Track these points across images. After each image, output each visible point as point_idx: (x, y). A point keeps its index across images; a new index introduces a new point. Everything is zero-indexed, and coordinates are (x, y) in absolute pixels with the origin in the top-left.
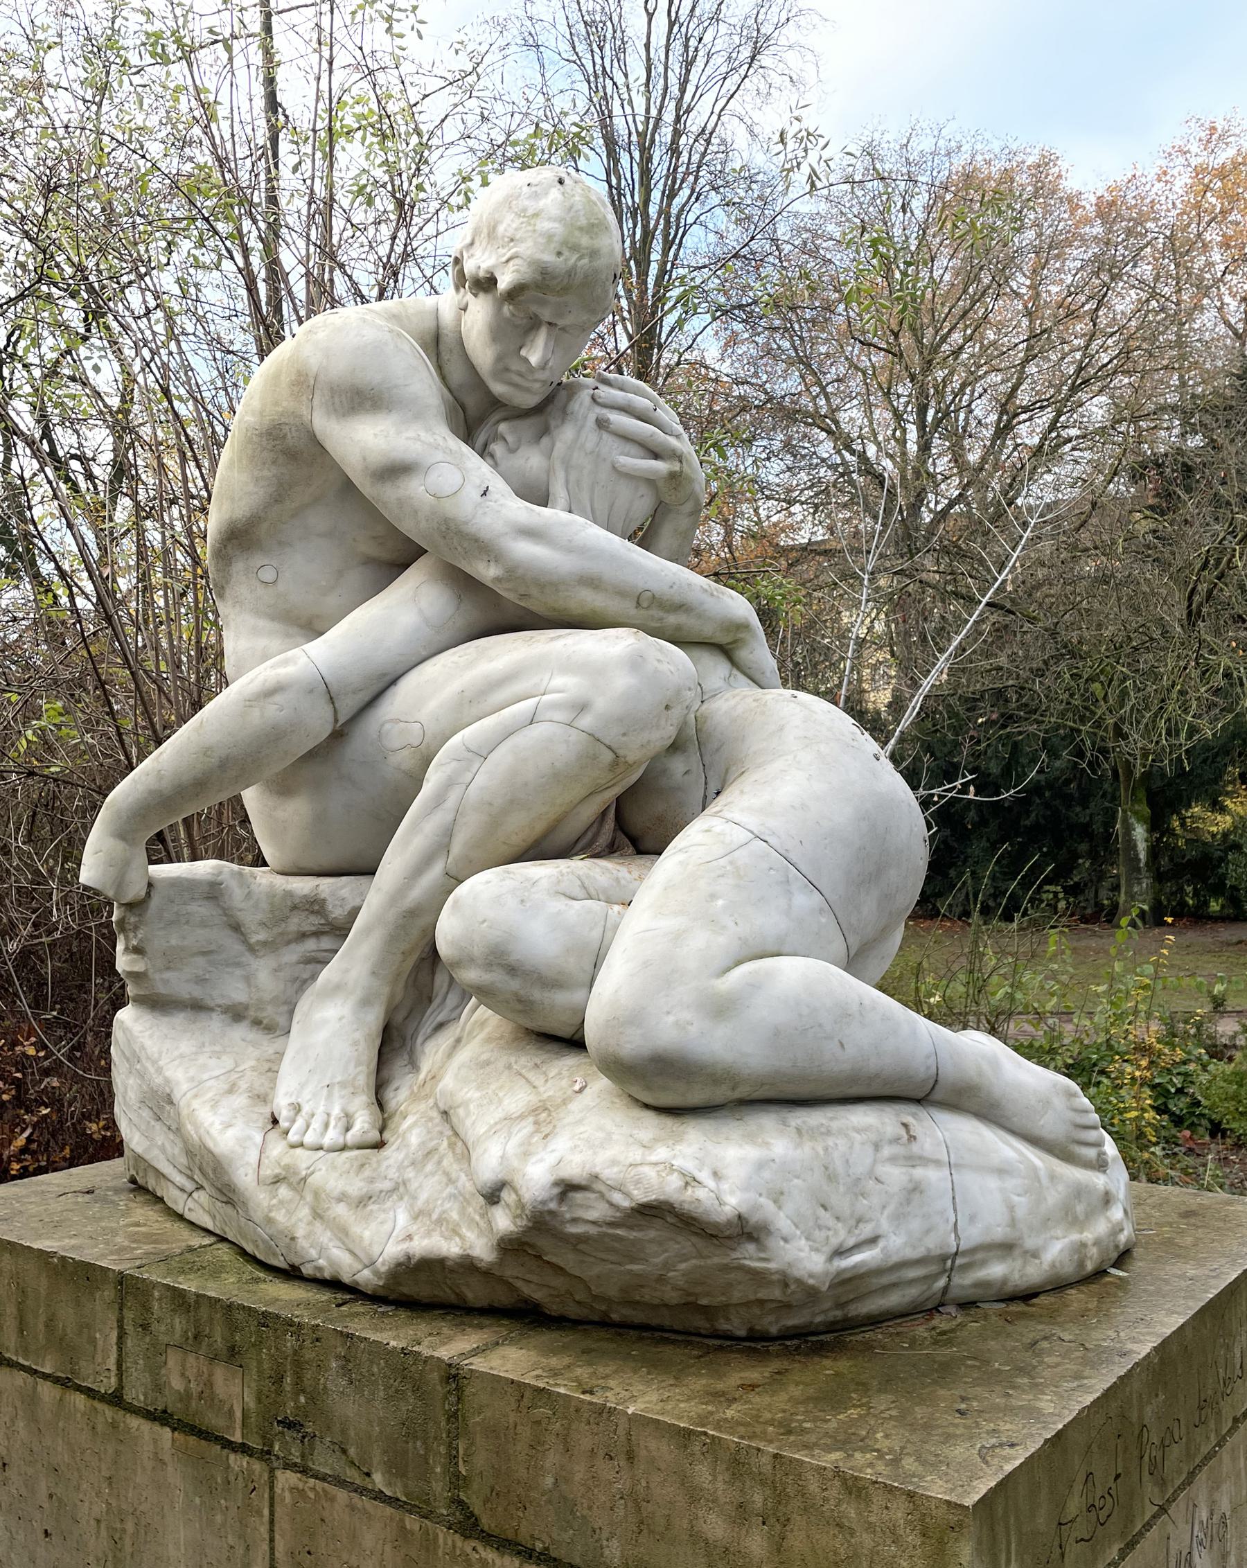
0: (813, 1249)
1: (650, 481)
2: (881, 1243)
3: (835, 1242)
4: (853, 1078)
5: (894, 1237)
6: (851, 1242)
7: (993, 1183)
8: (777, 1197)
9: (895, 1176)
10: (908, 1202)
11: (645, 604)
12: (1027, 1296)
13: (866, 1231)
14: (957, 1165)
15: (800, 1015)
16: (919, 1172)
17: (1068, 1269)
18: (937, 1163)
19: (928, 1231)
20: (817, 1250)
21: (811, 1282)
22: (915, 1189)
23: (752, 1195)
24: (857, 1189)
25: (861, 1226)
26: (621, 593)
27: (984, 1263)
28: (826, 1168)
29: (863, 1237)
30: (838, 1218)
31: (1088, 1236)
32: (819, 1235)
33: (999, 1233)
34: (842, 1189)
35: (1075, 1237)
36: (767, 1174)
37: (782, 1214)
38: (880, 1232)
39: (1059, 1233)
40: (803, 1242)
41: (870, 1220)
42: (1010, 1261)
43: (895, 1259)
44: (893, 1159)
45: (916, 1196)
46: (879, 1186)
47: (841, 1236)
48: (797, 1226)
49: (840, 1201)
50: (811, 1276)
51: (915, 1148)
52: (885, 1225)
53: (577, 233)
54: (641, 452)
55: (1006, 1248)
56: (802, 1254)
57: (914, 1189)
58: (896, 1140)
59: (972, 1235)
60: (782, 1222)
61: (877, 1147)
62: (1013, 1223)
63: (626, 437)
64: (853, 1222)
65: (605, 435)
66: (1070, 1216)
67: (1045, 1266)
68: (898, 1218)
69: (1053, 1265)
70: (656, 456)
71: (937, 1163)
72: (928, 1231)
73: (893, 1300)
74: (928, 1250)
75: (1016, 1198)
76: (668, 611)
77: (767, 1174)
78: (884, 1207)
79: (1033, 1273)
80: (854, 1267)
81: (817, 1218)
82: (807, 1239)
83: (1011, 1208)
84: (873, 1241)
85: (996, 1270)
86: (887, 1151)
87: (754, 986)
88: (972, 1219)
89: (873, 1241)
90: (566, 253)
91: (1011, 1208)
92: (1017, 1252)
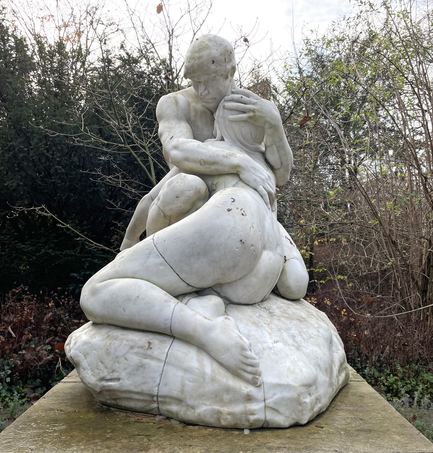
0: (93, 375)
1: (245, 121)
2: (121, 381)
3: (102, 375)
4: (140, 323)
5: (127, 381)
6: (109, 377)
7: (180, 373)
8: (86, 355)
9: (135, 359)
10: (137, 370)
11: (203, 164)
12: (187, 423)
13: (115, 375)
14: (168, 363)
15: (112, 298)
16: (147, 361)
17: (211, 420)
18: (159, 360)
19: (144, 383)
20: (94, 376)
21: (90, 385)
22: (142, 366)
23: (77, 352)
24: (116, 359)
25: (114, 373)
26: (195, 161)
27: (170, 404)
28: (107, 350)
29: (113, 377)
30: (106, 368)
31: (225, 409)
32: (96, 371)
33: (175, 393)
34: (110, 358)
35: (217, 407)
36: (85, 347)
37: (85, 361)
38: (121, 377)
39: (208, 403)
40: (89, 372)
41: (118, 372)
42: (180, 406)
43: (125, 388)
44: (137, 354)
45: (142, 369)
46: (126, 361)
47: (105, 373)
48: (89, 366)
49: (108, 362)
50: (89, 383)
51: (149, 352)
52: (123, 375)
53: (194, 54)
54: (237, 113)
55: (179, 401)
56: (88, 375)
57: (141, 366)
58: (142, 347)
59: (164, 391)
60: (84, 363)
61: (132, 348)
62: (182, 391)
63: (231, 109)
64: (111, 371)
65: (225, 111)
66: (217, 397)
67: (196, 414)
68: (131, 374)
69: (199, 415)
70: (244, 112)
71: (159, 360)
72: (144, 383)
73: (132, 404)
74: (143, 390)
75: (187, 382)
76: (211, 165)
77: (85, 347)
78: (125, 369)
79: (191, 415)
80: (108, 386)
81: (98, 365)
82: (92, 371)
83: (183, 386)
84: (118, 379)
85: (174, 408)
86: (135, 350)
87: (105, 286)
88: (166, 384)
89: (118, 379)
90: (191, 61)
91: (183, 386)
92: (183, 404)
